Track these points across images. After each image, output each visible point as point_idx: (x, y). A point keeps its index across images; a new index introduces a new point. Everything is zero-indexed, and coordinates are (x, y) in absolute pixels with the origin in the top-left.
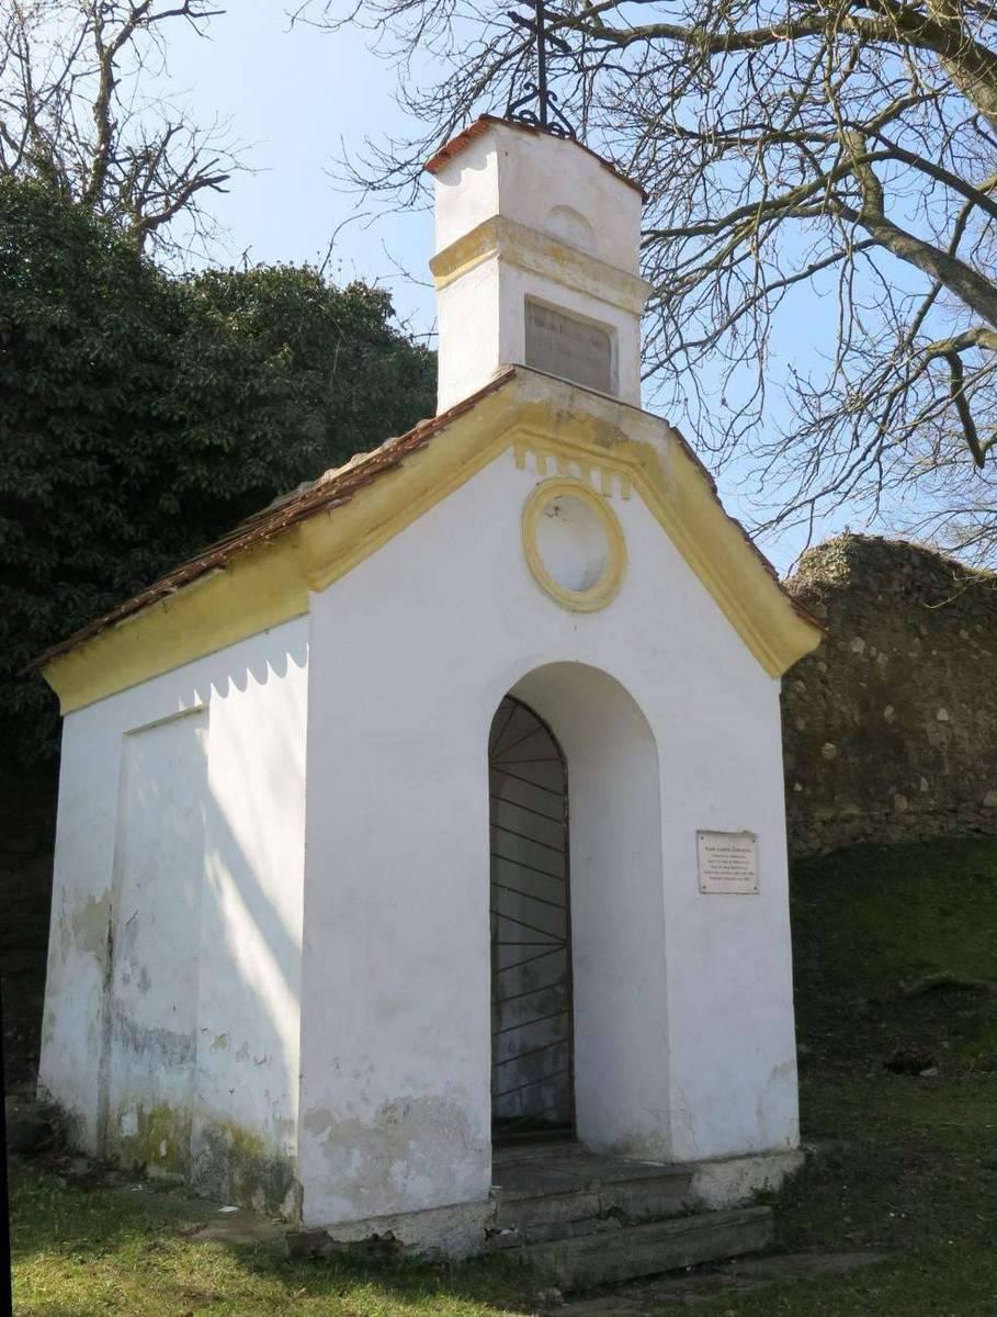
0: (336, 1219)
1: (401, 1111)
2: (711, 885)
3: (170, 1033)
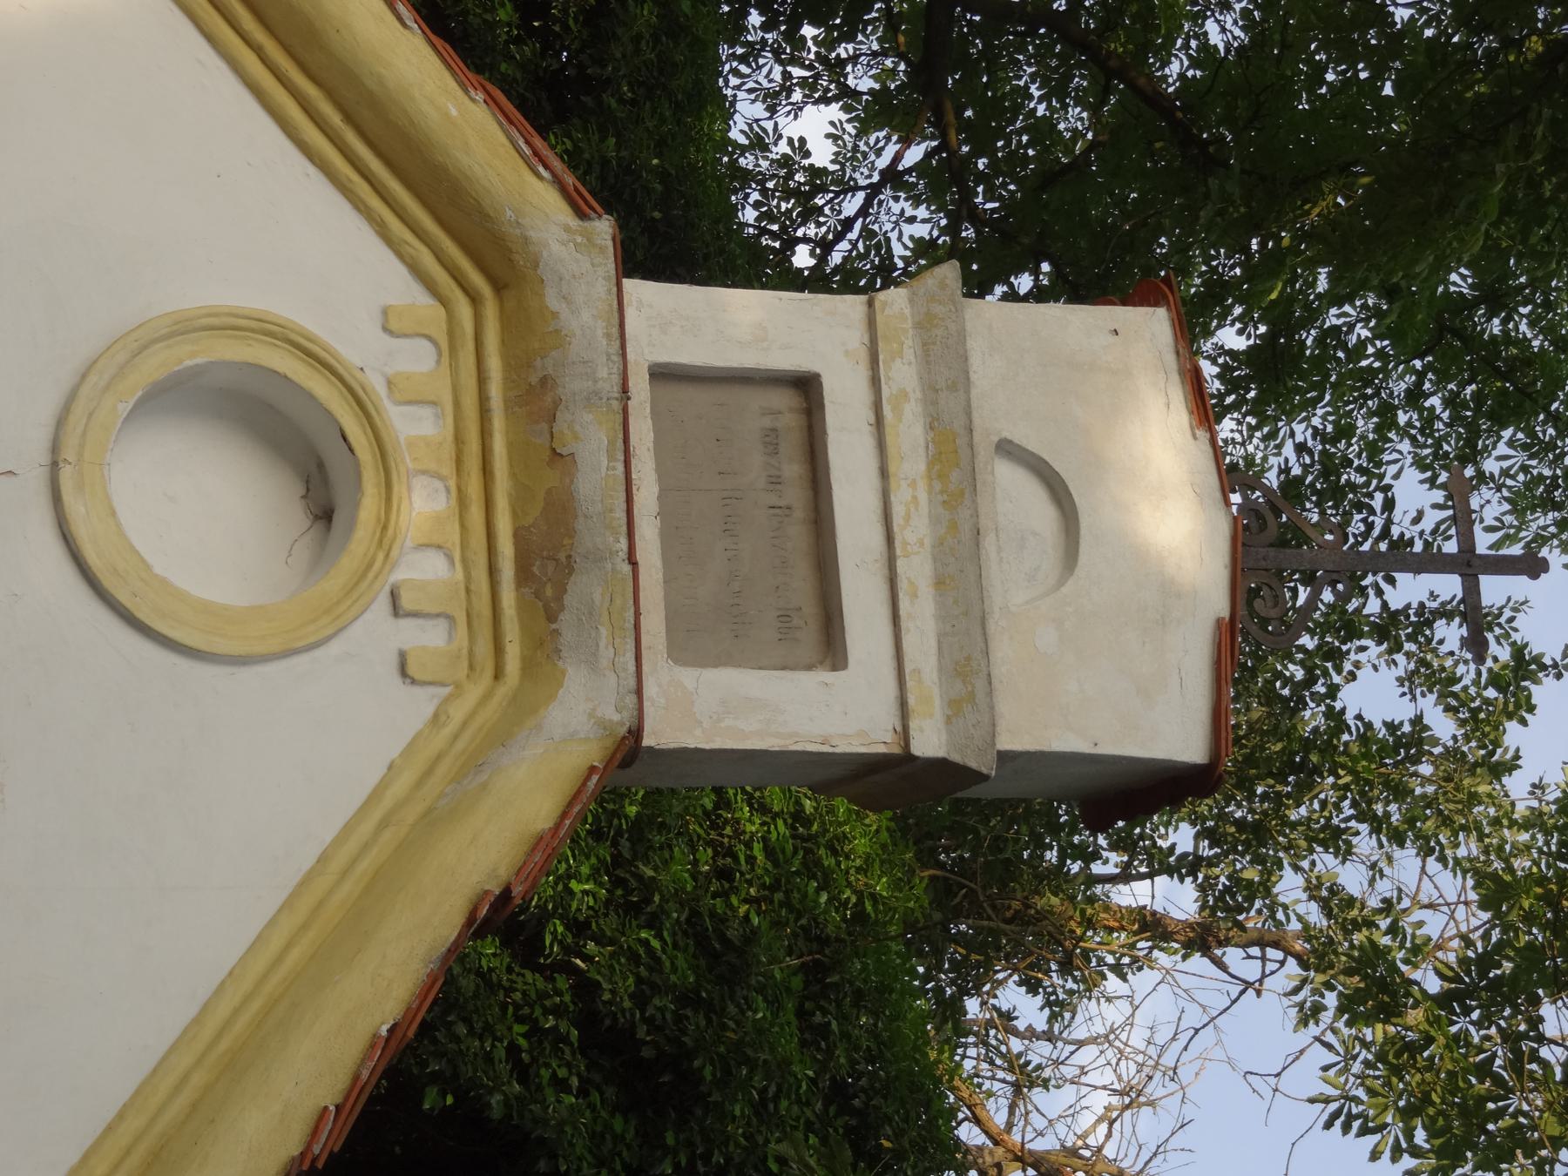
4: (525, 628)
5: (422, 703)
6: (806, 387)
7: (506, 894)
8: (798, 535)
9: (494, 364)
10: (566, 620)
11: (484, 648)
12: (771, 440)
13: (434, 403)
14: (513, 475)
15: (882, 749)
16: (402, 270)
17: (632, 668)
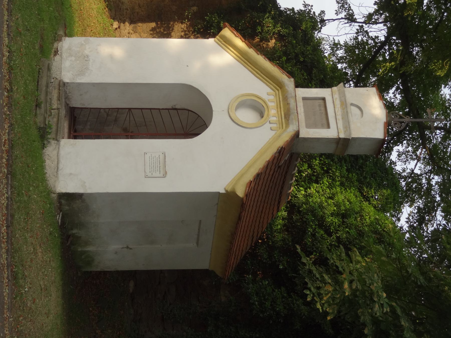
0: (64, 45)
1: (87, 59)
2: (147, 156)
4: (285, 123)
5: (274, 133)
6: (324, 99)
7: (282, 147)
8: (324, 116)
9: (281, 97)
10: (290, 121)
11: (281, 126)
12: (320, 106)
13: (274, 102)
14: (283, 108)
15: (336, 137)
16: (269, 89)
17: (298, 124)
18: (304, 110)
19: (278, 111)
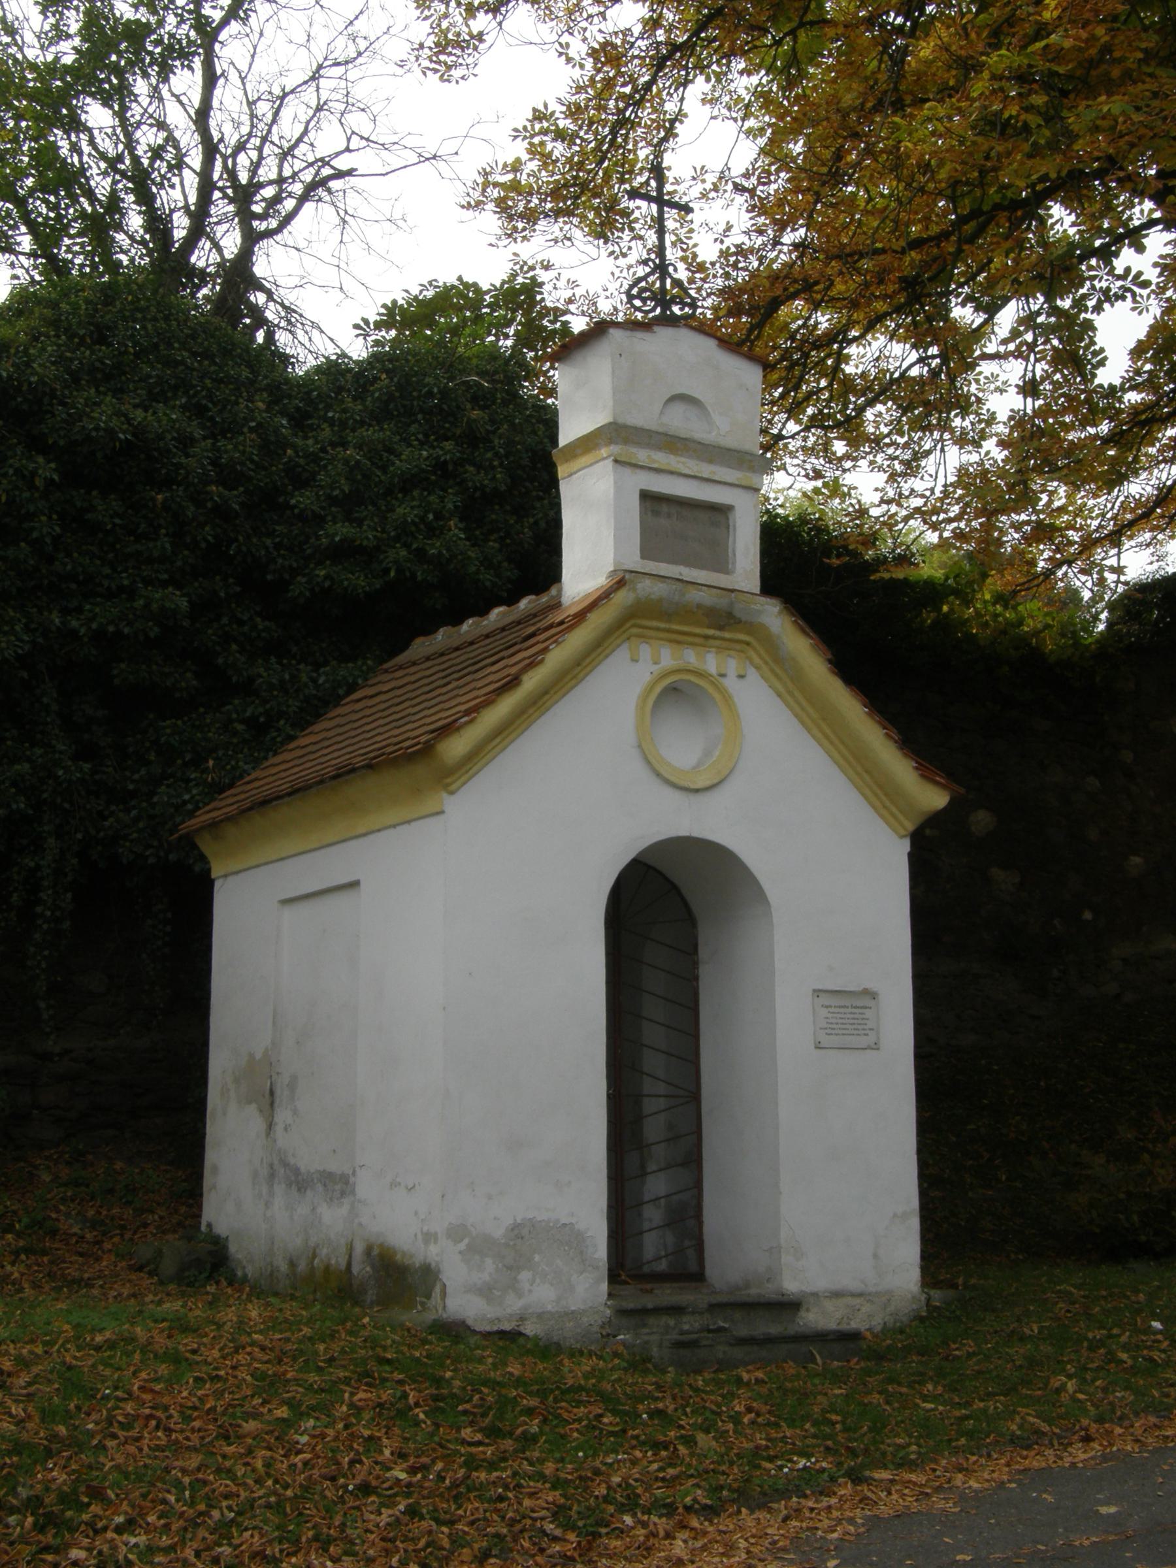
2: (826, 1041)
3: (330, 1173)
7: (830, 661)
9: (655, 624)
11: (738, 647)
18: (866, 696)
19: (692, 644)
